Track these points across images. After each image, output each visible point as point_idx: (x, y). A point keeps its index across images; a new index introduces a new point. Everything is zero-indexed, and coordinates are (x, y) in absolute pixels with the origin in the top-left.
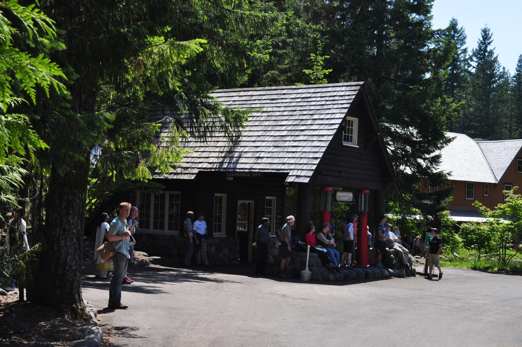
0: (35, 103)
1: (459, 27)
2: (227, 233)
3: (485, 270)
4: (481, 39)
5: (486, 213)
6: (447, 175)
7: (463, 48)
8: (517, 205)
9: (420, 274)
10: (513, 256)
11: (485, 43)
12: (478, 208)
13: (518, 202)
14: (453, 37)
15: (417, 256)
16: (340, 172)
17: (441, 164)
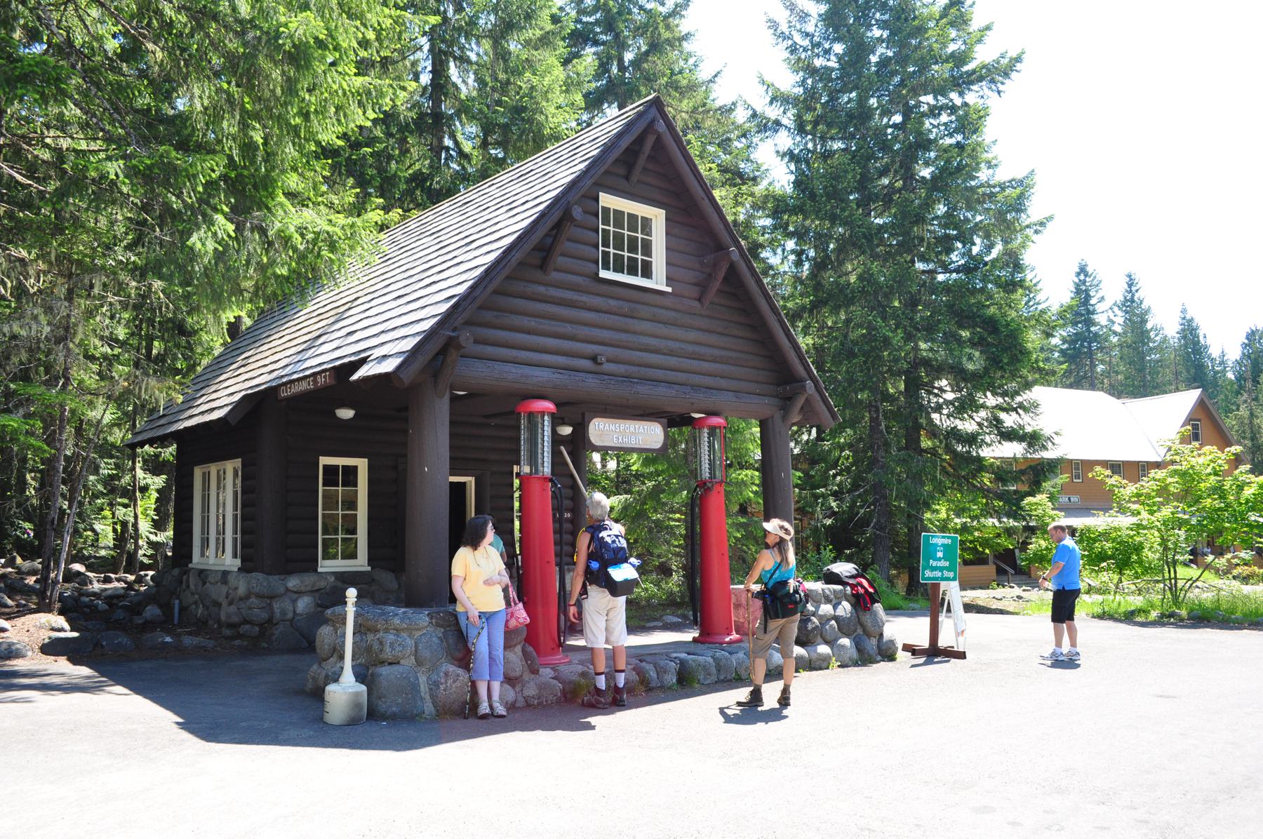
0: (355, 377)
1: (1089, 269)
2: (371, 561)
3: (1129, 617)
4: (1126, 286)
5: (1122, 490)
6: (1053, 435)
7: (1099, 295)
8: (1192, 467)
9: (912, 650)
10: (1195, 581)
11: (1131, 291)
12: (1103, 483)
13: (1193, 461)
14: (1084, 282)
15: (1024, 588)
16: (594, 359)
17: (1040, 416)
